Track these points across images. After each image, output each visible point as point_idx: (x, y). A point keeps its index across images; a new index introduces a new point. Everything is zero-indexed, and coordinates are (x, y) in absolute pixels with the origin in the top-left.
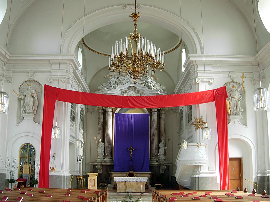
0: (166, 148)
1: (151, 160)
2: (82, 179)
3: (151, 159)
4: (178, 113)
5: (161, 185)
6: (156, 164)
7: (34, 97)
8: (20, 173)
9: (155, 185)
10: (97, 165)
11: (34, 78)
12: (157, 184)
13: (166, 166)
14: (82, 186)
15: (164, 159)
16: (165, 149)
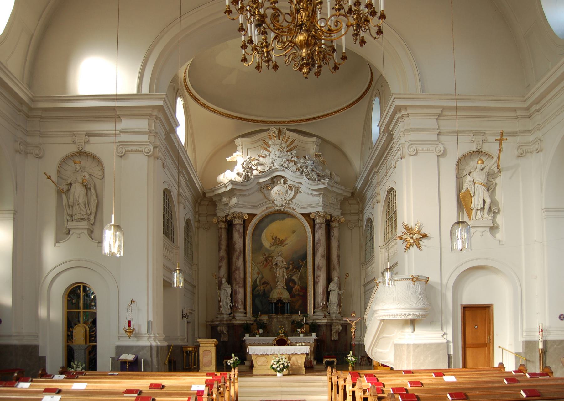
0: (342, 292)
1: (315, 314)
2: (192, 353)
3: (314, 312)
4: (363, 226)
6: (324, 321)
7: (89, 186)
8: (68, 342)
9: (324, 362)
10: (218, 325)
11: (88, 149)
12: (328, 360)
13: (342, 325)
14: (192, 366)
15: (339, 313)
16: (339, 294)
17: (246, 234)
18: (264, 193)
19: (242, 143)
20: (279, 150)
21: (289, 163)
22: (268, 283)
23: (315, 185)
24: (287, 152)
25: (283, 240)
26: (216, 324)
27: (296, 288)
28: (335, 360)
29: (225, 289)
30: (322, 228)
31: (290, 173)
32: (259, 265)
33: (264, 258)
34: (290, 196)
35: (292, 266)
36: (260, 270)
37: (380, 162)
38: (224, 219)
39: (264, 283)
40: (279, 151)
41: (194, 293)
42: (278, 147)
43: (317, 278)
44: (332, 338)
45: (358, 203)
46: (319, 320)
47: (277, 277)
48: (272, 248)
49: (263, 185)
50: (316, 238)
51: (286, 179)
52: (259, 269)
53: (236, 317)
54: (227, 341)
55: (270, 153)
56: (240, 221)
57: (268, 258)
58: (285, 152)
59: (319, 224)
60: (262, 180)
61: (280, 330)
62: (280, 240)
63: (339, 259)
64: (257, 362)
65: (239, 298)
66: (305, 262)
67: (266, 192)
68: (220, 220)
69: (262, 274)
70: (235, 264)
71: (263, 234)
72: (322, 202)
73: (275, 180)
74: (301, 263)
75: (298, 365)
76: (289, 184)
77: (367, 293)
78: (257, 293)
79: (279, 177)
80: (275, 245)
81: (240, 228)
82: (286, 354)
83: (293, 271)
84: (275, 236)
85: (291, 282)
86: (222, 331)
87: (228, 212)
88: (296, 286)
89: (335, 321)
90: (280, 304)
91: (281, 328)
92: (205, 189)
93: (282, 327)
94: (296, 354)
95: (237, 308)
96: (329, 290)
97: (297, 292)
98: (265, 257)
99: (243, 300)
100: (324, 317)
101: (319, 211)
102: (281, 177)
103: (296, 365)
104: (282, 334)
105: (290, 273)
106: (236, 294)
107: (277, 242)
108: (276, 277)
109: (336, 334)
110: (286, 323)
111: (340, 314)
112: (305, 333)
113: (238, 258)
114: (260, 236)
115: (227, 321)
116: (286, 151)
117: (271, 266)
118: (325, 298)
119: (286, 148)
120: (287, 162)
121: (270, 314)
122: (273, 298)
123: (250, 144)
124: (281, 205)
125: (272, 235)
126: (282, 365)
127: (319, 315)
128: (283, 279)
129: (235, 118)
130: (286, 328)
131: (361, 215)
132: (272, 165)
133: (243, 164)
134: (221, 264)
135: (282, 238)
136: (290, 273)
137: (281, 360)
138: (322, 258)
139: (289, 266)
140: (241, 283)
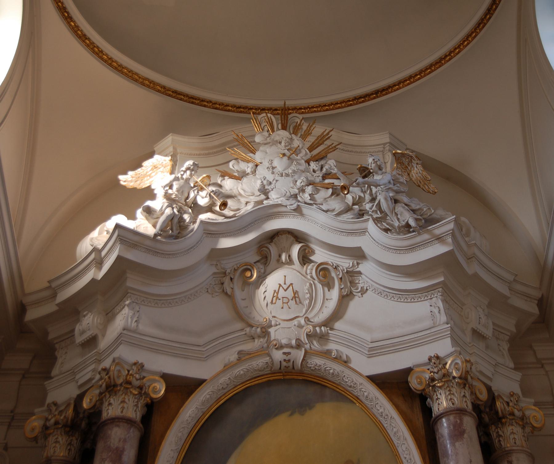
19: (175, 149)
20: (284, 155)
21: (318, 191)
23: (411, 248)
24: (308, 162)
30: (465, 436)
31: (322, 218)
34: (324, 308)
40: (285, 158)
42: (282, 148)
49: (229, 264)
55: (257, 166)
58: (303, 161)
60: (226, 243)
67: (239, 294)
72: (444, 318)
73: (273, 249)
76: (319, 262)
81: (125, 441)
116: (306, 158)
119: (303, 152)
123: (199, 155)
124: (294, 342)
129: (163, 90)
132: (263, 197)
133: (171, 187)
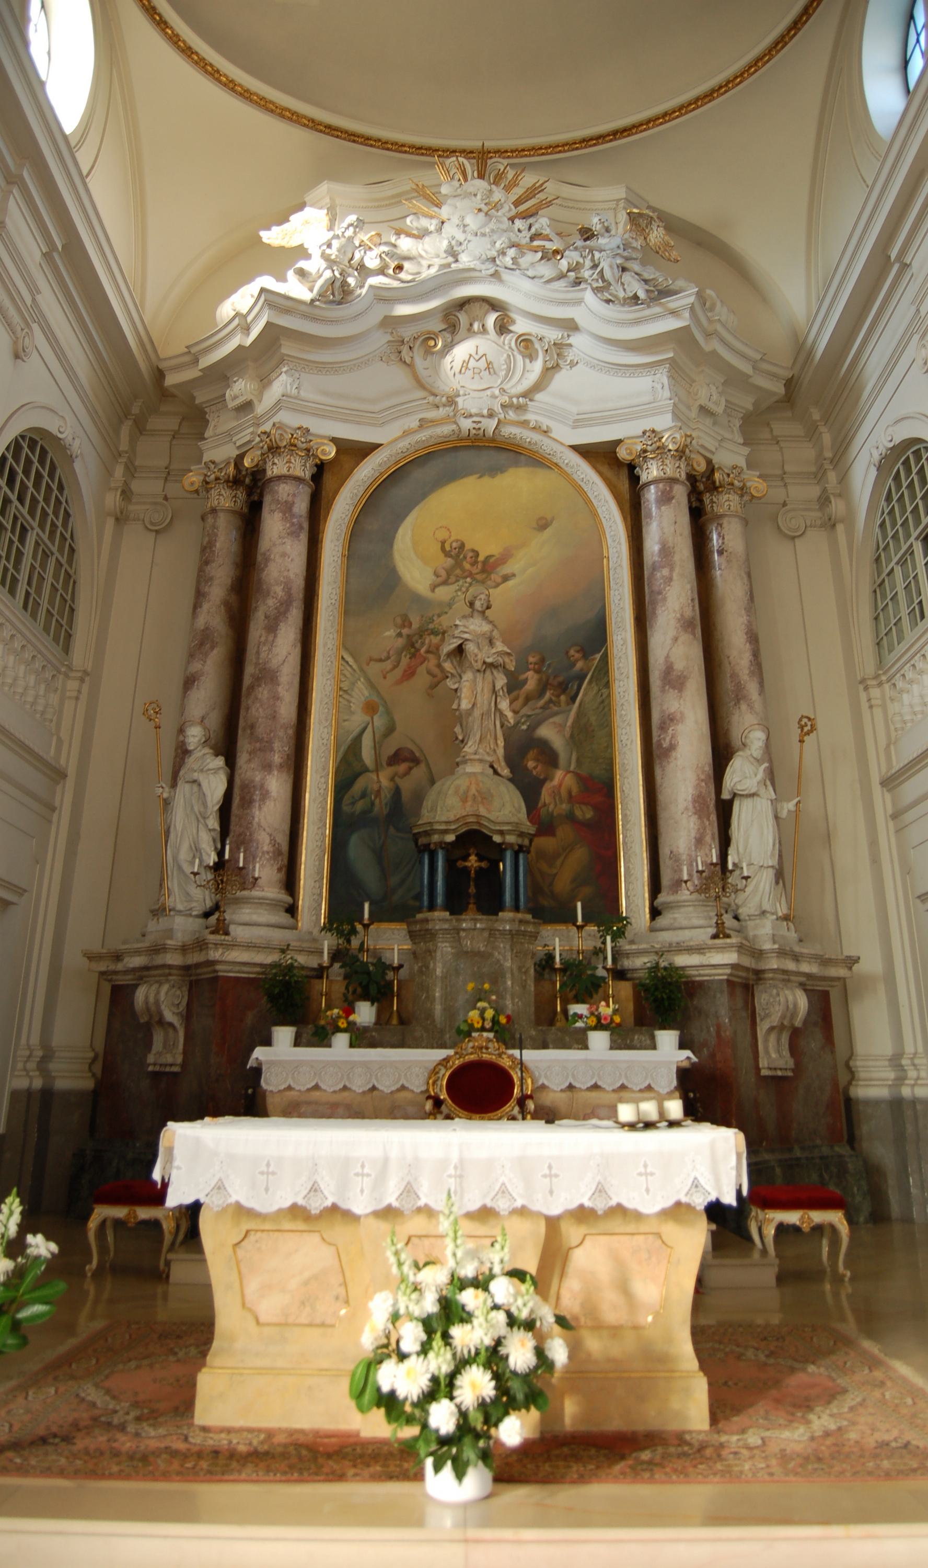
1: (661, 921)
3: (655, 913)
5: (102, 1212)
10: (143, 974)
12: (792, 1217)
13: (802, 985)
17: (321, 527)
18: (410, 366)
21: (523, 254)
22: (417, 754)
23: (637, 322)
24: (512, 219)
25: (492, 560)
26: (134, 970)
27: (556, 782)
28: (835, 1217)
29: (195, 776)
31: (526, 285)
32: (374, 669)
33: (400, 635)
35: (536, 676)
36: (378, 692)
37: (848, 354)
38: (231, 470)
39: (396, 758)
40: (482, 215)
41: (53, 809)
42: (478, 202)
43: (663, 728)
44: (763, 1063)
45: (812, 433)
46: (690, 950)
47: (461, 716)
48: (444, 593)
49: (407, 332)
50: (652, 546)
51: (507, 315)
52: (371, 685)
53: (232, 928)
54: (176, 1069)
56: (301, 468)
57: (421, 636)
59: (661, 485)
61: (474, 1008)
62: (481, 558)
63: (756, 654)
64: (252, 1287)
65: (260, 826)
66: (598, 656)
67: (419, 363)
68: (213, 477)
69: (388, 712)
70: (258, 653)
71: (401, 531)
73: (463, 318)
74: (580, 665)
75: (636, 1328)
77: (910, 816)
78: (359, 806)
79: (477, 305)
80: (457, 581)
81: (294, 495)
82: (522, 1212)
83: (542, 702)
84: (457, 541)
85: (532, 754)
86: (153, 1008)
87: (247, 438)
88: (559, 774)
89: (774, 964)
90: (473, 858)
91: (480, 995)
92: (161, 356)
93: (486, 986)
94: (619, 1210)
95: (247, 881)
96: (726, 796)
97: (565, 806)
98: (405, 631)
99: (283, 840)
100: (715, 937)
101: (657, 429)
102: (487, 307)
103: (615, 1331)
104: (483, 1029)
105: (526, 711)
106: (247, 803)
107: (467, 566)
108: (460, 718)
109: (779, 1040)
110: (508, 964)
111: (791, 924)
112: (619, 1025)
113: (272, 628)
114: (388, 540)
115: (184, 949)
116: (509, 215)
117: (434, 676)
118: (709, 832)
120: (513, 250)
121: (420, 910)
122: (437, 819)
124: (485, 412)
125: (442, 535)
126: (487, 1365)
127: (685, 923)
128: (492, 727)
129: (311, 124)
130: (508, 997)
131: (832, 477)
132: (450, 259)
133: (329, 246)
134: (196, 666)
135: (488, 548)
136: (526, 711)
137: (469, 1298)
138: (686, 631)
139: (523, 677)
140: (280, 751)
